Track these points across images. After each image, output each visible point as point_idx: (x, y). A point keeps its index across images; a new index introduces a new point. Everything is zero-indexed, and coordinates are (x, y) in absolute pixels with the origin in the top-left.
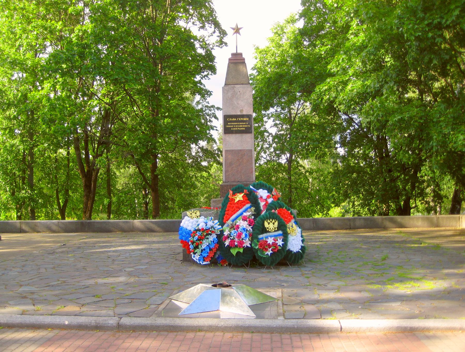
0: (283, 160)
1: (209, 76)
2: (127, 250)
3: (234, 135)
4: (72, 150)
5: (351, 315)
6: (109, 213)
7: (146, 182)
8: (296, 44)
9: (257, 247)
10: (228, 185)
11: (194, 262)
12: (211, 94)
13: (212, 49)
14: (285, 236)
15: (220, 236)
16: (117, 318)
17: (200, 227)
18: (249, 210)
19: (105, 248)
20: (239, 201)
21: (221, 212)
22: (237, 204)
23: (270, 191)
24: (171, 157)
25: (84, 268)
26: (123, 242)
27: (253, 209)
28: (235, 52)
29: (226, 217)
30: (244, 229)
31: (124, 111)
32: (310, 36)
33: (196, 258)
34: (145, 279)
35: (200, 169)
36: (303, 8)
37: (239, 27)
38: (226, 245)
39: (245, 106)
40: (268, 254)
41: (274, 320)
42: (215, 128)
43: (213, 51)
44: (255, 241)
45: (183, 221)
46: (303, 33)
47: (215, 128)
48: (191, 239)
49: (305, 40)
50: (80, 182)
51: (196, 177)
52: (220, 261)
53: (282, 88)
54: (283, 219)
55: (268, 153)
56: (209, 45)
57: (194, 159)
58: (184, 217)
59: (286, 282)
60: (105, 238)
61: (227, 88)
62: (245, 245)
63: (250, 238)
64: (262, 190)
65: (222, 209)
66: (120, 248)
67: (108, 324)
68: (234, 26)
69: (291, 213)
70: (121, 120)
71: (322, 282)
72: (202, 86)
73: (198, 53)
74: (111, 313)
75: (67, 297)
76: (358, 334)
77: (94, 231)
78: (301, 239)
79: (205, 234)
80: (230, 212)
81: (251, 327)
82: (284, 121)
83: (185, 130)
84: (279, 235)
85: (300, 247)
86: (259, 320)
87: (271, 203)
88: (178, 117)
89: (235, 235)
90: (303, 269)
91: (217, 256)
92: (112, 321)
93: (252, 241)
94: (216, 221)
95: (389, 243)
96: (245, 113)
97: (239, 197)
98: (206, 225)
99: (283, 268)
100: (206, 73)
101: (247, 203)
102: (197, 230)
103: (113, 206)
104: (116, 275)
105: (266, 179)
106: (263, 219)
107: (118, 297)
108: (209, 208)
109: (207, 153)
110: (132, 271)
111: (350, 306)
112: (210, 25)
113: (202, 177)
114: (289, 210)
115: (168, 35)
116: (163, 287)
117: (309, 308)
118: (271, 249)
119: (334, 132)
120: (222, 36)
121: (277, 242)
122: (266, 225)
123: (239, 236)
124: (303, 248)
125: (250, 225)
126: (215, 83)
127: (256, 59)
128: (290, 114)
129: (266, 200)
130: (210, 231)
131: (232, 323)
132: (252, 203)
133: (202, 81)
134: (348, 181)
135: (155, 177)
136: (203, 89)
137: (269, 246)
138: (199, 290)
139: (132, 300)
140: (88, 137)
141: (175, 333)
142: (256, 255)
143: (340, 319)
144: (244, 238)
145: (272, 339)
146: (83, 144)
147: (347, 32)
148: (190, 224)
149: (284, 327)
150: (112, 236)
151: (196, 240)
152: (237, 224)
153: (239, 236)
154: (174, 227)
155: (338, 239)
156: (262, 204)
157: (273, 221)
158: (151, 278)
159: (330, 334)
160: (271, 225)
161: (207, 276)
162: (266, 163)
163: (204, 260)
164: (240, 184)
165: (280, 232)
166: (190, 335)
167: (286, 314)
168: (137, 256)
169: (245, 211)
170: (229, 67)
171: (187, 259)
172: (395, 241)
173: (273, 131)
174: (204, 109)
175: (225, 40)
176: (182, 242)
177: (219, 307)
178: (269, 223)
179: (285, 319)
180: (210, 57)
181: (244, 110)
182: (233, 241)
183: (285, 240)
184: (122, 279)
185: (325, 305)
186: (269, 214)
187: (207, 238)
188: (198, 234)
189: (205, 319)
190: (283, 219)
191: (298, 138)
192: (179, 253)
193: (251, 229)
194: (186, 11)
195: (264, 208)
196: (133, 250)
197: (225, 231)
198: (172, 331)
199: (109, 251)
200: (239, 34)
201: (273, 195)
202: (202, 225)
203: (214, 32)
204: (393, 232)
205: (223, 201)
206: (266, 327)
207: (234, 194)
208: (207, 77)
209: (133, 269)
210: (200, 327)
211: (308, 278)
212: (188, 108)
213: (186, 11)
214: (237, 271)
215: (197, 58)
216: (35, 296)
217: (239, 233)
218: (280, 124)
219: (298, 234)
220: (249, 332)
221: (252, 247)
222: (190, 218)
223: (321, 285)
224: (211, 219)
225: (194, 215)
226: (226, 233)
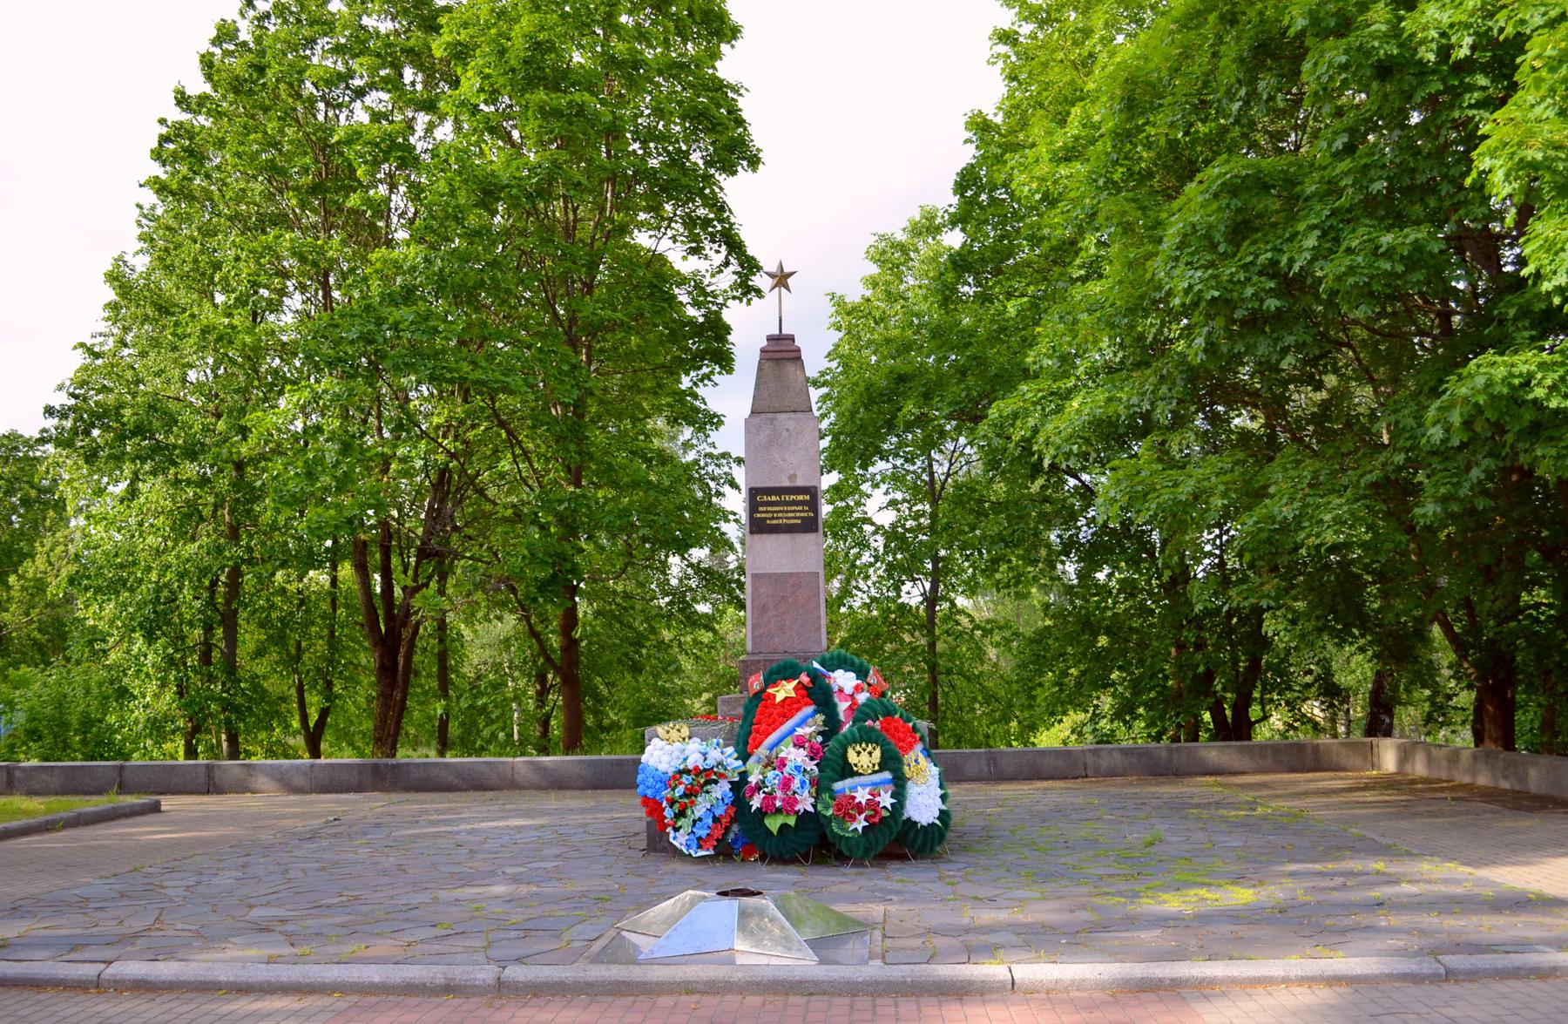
0: (912, 594)
1: (716, 378)
3: (774, 536)
4: (346, 570)
7: (548, 659)
9: (830, 812)
11: (676, 852)
12: (721, 423)
14: (899, 785)
15: (740, 786)
21: (741, 727)
23: (862, 673)
24: (615, 592)
25: (401, 869)
27: (820, 718)
30: (797, 768)
33: (679, 840)
37: (787, 270)
39: (806, 459)
42: (731, 517)
44: (826, 796)
46: (961, 263)
47: (731, 517)
48: (667, 793)
50: (367, 658)
51: (680, 645)
56: (715, 297)
57: (674, 595)
61: (757, 420)
62: (800, 807)
65: (745, 719)
70: (481, 492)
71: (984, 892)
72: (697, 403)
75: (367, 928)
77: (408, 789)
78: (940, 792)
80: (764, 726)
82: (916, 493)
85: (937, 814)
87: (864, 705)
90: (943, 867)
91: (731, 836)
92: (485, 974)
94: (730, 750)
96: (800, 483)
97: (784, 691)
99: (896, 865)
100: (705, 370)
102: (681, 772)
105: (866, 644)
108: (710, 716)
109: (713, 579)
111: (1037, 940)
112: (715, 246)
113: (696, 642)
119: (1047, 521)
122: (852, 757)
123: (786, 784)
124: (944, 815)
125: (812, 759)
126: (730, 396)
127: (839, 329)
128: (932, 474)
129: (852, 696)
134: (1081, 649)
135: (570, 645)
136: (697, 410)
137: (860, 808)
139: (527, 932)
140: (391, 537)
141: (631, 999)
145: (852, 1007)
146: (378, 556)
148: (665, 758)
153: (786, 784)
154: (623, 777)
156: (843, 706)
157: (870, 748)
159: (988, 997)
160: (864, 758)
162: (867, 606)
163: (700, 847)
164: (789, 658)
165: (887, 775)
166: (666, 1001)
170: (760, 369)
171: (657, 843)
173: (887, 518)
178: (859, 753)
180: (716, 330)
181: (799, 475)
182: (770, 797)
183: (899, 794)
184: (500, 889)
192: (636, 834)
194: (655, 209)
199: (458, 833)
202: (694, 760)
203: (727, 264)
209: (521, 869)
210: (689, 983)
215: (681, 330)
216: (290, 927)
218: (904, 500)
221: (817, 813)
225: (674, 733)
226: (753, 779)
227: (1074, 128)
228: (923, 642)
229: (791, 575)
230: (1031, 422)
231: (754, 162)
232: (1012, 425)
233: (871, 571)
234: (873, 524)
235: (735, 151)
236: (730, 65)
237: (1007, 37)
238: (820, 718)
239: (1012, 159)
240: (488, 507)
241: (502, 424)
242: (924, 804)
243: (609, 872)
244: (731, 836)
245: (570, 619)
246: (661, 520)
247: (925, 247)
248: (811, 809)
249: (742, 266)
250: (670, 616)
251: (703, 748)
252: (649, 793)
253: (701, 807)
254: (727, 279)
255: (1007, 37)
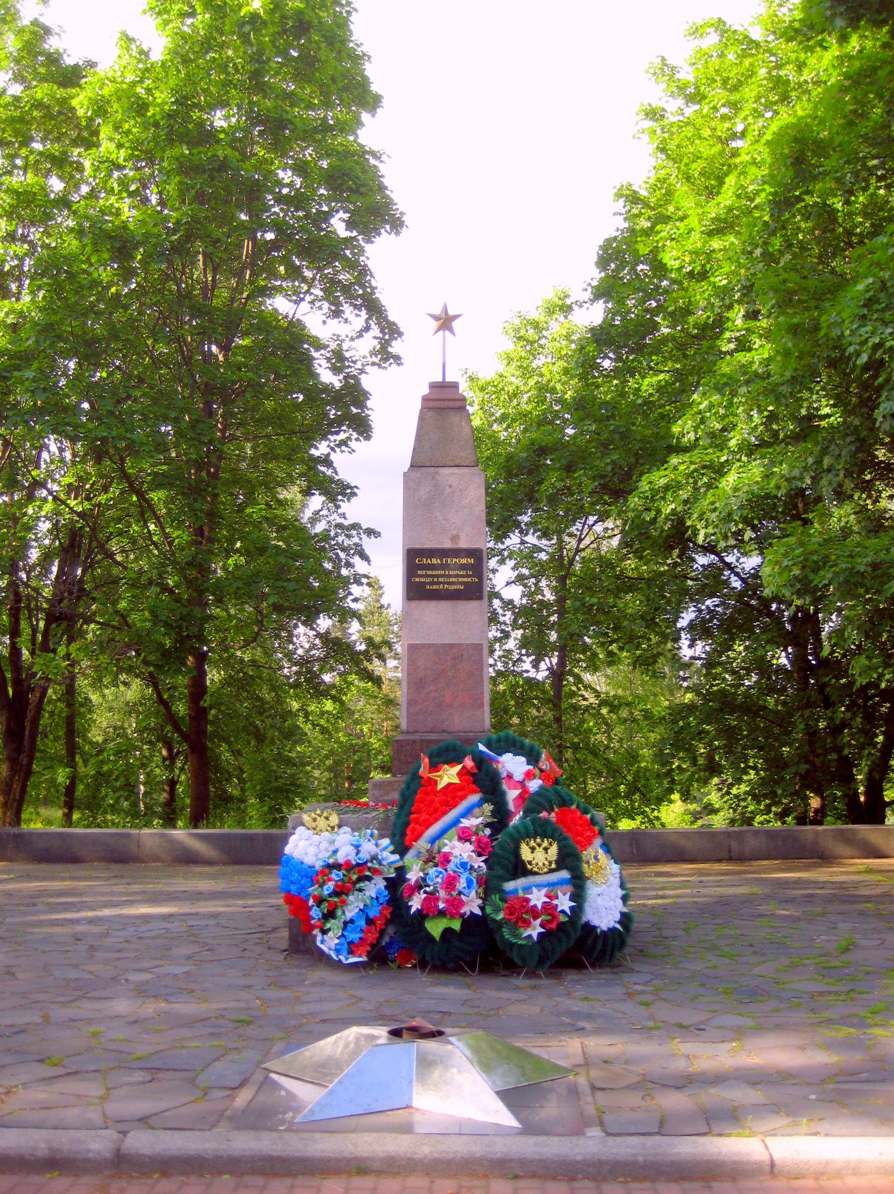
1: (353, 444)
2: (128, 917)
5: (795, 1124)
6: (70, 806)
8: (585, 366)
9: (500, 916)
10: (414, 742)
11: (322, 956)
13: (362, 371)
14: (578, 887)
15: (396, 883)
16: (111, 1134)
17: (341, 858)
18: (477, 811)
19: (66, 910)
20: (449, 784)
21: (398, 815)
22: (444, 794)
23: (533, 757)
24: (242, 660)
26: (112, 893)
27: (488, 808)
28: (441, 380)
29: (413, 831)
30: (463, 865)
31: (121, 533)
32: (619, 347)
33: (328, 943)
34: (185, 1008)
35: (320, 691)
36: (603, 274)
37: (451, 313)
38: (413, 910)
40: (530, 936)
41: (574, 1139)
43: (363, 377)
45: (292, 839)
46: (602, 337)
48: (314, 890)
49: (606, 357)
51: (307, 715)
52: (394, 954)
53: (546, 483)
54: (569, 835)
55: (498, 653)
56: (354, 362)
58: (294, 828)
59: (589, 1017)
60: (64, 879)
61: (417, 474)
62: (465, 910)
63: (481, 890)
64: (510, 755)
65: (402, 807)
66: (107, 912)
67: (88, 1151)
68: (438, 311)
69: (592, 819)
71: (689, 1017)
73: (322, 383)
74: (95, 1116)
76: (822, 1183)
78: (620, 892)
79: (354, 877)
80: (424, 816)
81: (510, 1160)
83: (285, 584)
84: (561, 883)
86: (531, 1140)
87: (537, 793)
88: (262, 551)
89: (439, 880)
90: (627, 978)
91: (386, 939)
92: (99, 1144)
93: (485, 898)
94: (385, 842)
95: (844, 898)
96: (463, 544)
97: (449, 776)
98: (358, 853)
99: (571, 976)
100: (342, 436)
101: (474, 792)
103: (81, 787)
104: (103, 993)
106: (517, 836)
107: (111, 1065)
110: (148, 982)
114: (587, 813)
115: (245, 334)
116: (241, 1031)
117: (673, 1101)
118: (539, 921)
120: (387, 337)
121: (555, 902)
122: (525, 853)
123: (450, 883)
124: (625, 919)
125: (480, 855)
129: (522, 783)
130: (369, 869)
131: (459, 1147)
132: (485, 793)
133: (333, 457)
135: (199, 714)
136: (331, 480)
137: (535, 912)
138: (352, 1046)
139: (155, 1070)
141: (288, 1181)
142: (497, 937)
143: (767, 1134)
144: (465, 891)
147: (718, 337)
148: (312, 850)
149: (607, 1162)
150: (82, 873)
151: (330, 895)
152: (445, 850)
153: (450, 883)
155: (705, 891)
156: (512, 795)
157: (545, 844)
158: (205, 1006)
160: (539, 854)
161: (360, 999)
163: (351, 952)
165: (565, 874)
167: (606, 1118)
168: (158, 936)
169: (467, 813)
170: (422, 418)
172: (861, 896)
174: (332, 534)
175: (396, 347)
176: (290, 899)
177: (410, 1098)
178: (533, 849)
179: (608, 1134)
180: (353, 395)
182: (432, 897)
183: (578, 896)
184: (122, 1006)
185: (714, 1091)
186: (533, 822)
187: (360, 890)
188: (333, 876)
189: (375, 1135)
190: (569, 835)
191: (586, 611)
192: (275, 929)
193: (482, 864)
195: (517, 807)
196: (146, 918)
197: (410, 869)
198: (276, 1175)
199: (77, 921)
200: (452, 332)
201: (542, 771)
204: (852, 870)
205: (403, 786)
206: (554, 1162)
207: (435, 767)
208: (347, 446)
209: (149, 976)
211: (647, 1004)
212: (294, 530)
213: (294, 273)
214: (446, 985)
215: (318, 394)
217: (449, 876)
219: (611, 878)
220: (504, 1176)
222: (311, 832)
223: (686, 1027)
224: (372, 835)
225: (321, 822)
226: (413, 876)
227: (727, 198)
228: (550, 715)
229: (451, 646)
230: (684, 494)
231: (397, 225)
232: (664, 498)
233: (497, 646)
234: (501, 599)
235: (376, 213)
236: (371, 132)
237: (654, 114)
238: (488, 808)
239: (664, 230)
240: (115, 571)
241: (133, 489)
242: (604, 909)
243: (249, 981)
244: (386, 939)
245: (198, 687)
246: (291, 586)
247: (557, 326)
248: (478, 912)
249: (382, 331)
250: (297, 685)
251: (355, 838)
252: (293, 889)
253: (353, 907)
254: (369, 342)
255: (654, 114)
